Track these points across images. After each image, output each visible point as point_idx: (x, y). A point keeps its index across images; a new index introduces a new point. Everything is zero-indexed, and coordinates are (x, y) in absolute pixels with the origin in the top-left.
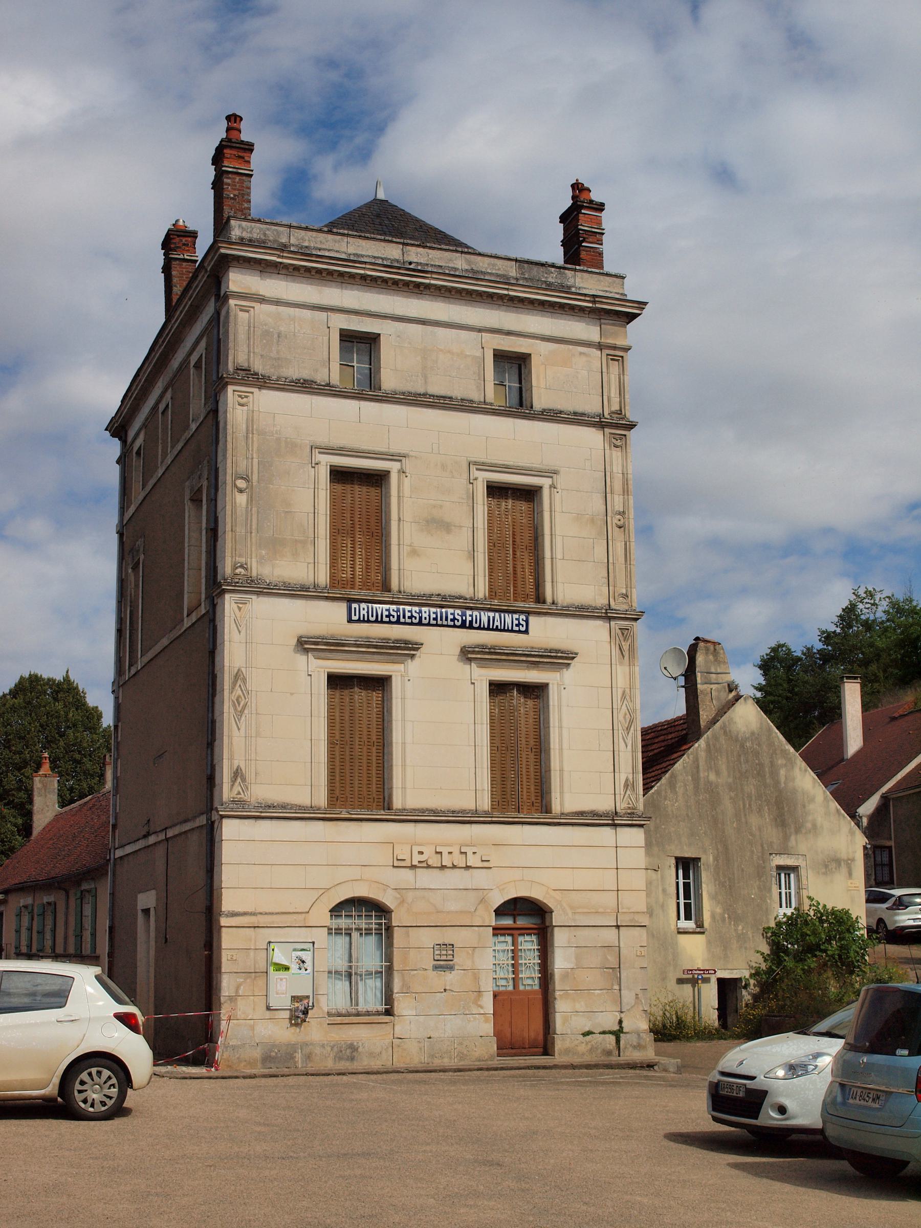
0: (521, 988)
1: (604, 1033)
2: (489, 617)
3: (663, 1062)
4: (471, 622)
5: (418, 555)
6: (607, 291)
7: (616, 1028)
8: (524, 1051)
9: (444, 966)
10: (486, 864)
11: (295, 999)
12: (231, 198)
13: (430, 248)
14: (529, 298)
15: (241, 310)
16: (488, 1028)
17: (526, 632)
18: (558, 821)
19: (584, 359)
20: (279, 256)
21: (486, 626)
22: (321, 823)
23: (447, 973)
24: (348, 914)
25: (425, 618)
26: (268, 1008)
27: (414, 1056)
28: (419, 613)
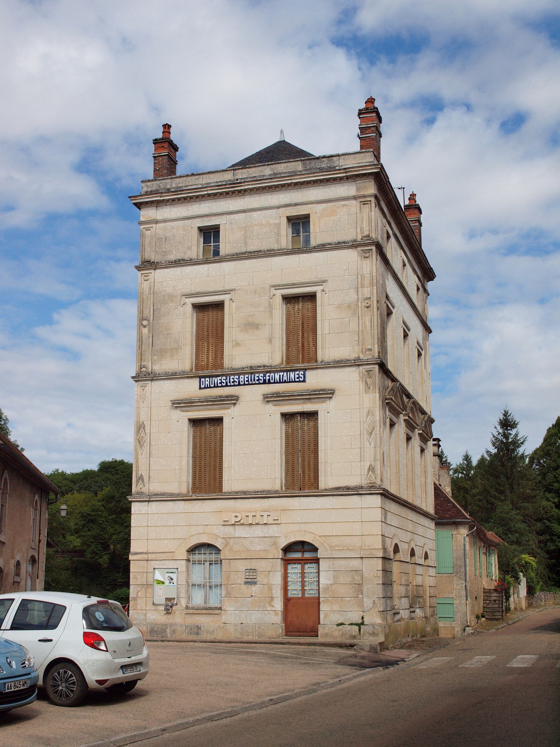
0: (306, 595)
1: (351, 624)
2: (280, 376)
3: (360, 644)
4: (269, 380)
5: (240, 346)
6: (359, 163)
7: (360, 621)
8: (306, 633)
9: (251, 582)
10: (276, 522)
11: (167, 599)
12: (158, 170)
13: (249, 168)
14: (300, 182)
15: (146, 230)
16: (278, 619)
17: (304, 381)
18: (321, 494)
19: (345, 209)
20: (161, 197)
21: (278, 381)
22: (182, 502)
23: (253, 586)
24: (199, 552)
25: (242, 381)
26: (154, 604)
27: (233, 634)
28: (238, 379)
